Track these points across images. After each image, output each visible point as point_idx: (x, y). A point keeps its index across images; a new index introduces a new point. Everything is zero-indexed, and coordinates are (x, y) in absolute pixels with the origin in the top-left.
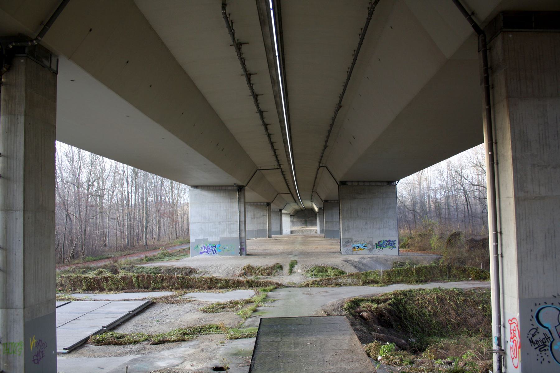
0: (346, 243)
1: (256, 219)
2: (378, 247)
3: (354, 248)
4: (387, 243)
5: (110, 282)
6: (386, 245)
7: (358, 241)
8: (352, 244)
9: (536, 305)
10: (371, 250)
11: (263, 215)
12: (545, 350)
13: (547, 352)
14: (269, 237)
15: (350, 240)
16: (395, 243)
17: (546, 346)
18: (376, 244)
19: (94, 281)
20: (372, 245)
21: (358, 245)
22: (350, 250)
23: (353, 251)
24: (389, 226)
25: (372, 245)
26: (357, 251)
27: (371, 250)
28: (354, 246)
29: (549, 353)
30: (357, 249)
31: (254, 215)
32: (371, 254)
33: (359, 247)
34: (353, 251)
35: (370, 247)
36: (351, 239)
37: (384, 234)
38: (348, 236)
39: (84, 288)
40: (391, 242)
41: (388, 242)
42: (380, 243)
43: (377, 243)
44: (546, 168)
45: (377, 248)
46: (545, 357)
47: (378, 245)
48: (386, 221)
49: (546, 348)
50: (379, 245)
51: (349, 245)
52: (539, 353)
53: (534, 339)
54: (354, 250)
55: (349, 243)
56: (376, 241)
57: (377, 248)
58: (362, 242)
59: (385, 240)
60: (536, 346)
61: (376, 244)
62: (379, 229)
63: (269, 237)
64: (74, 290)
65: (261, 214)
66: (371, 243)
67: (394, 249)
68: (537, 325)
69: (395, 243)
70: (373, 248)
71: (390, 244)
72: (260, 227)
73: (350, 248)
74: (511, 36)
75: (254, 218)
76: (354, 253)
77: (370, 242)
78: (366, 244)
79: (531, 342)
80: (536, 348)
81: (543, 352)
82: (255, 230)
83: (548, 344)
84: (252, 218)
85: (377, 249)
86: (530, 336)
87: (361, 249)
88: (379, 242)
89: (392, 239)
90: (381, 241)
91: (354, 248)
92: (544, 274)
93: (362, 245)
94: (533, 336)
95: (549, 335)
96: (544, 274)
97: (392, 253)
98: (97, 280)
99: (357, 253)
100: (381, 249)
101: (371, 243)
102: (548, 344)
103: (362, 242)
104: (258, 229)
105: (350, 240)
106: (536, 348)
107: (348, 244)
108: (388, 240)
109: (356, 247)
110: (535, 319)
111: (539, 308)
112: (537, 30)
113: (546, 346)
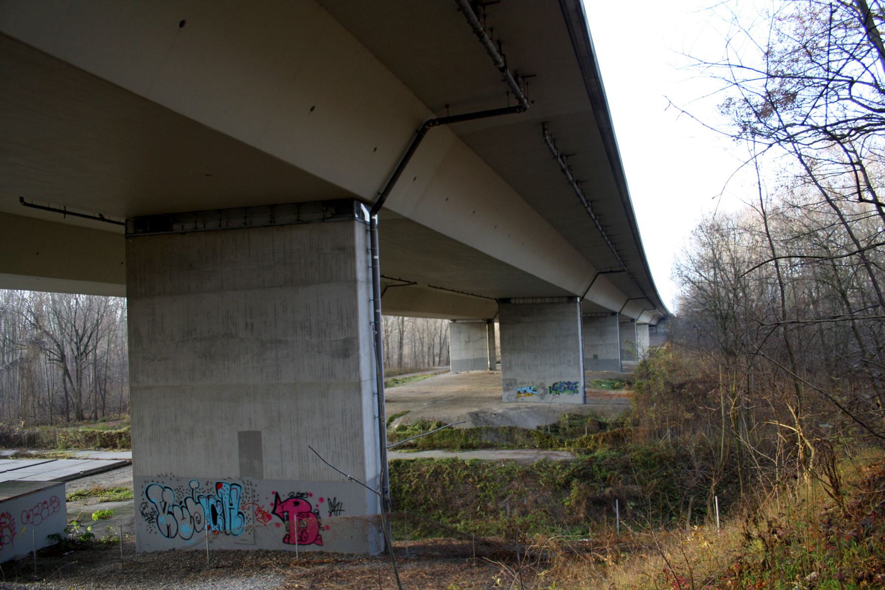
0: (507, 385)
1: (471, 343)
2: (553, 391)
3: (519, 392)
4: (565, 385)
5: (124, 439)
6: (565, 388)
7: (525, 383)
8: (515, 387)
9: (145, 482)
10: (542, 396)
11: (482, 338)
12: (153, 522)
13: (154, 524)
14: (491, 369)
15: (513, 382)
16: (577, 387)
17: (153, 518)
18: (550, 387)
19: (108, 437)
20: (544, 388)
21: (524, 389)
22: (513, 395)
23: (517, 397)
24: (569, 361)
25: (544, 388)
26: (523, 398)
27: (542, 396)
28: (519, 389)
29: (155, 524)
30: (523, 395)
31: (469, 337)
32: (543, 401)
33: (525, 391)
34: (517, 397)
35: (541, 391)
36: (513, 379)
37: (561, 373)
38: (509, 375)
39: (98, 444)
40: (571, 385)
41: (567, 384)
42: (556, 386)
43: (551, 385)
44: (153, 361)
45: (551, 392)
46: (153, 528)
47: (553, 389)
48: (564, 355)
49: (153, 520)
50: (555, 389)
51: (511, 389)
52: (148, 524)
53: (145, 512)
54: (519, 395)
55: (512, 385)
56: (549, 384)
57: (551, 392)
58: (531, 384)
59: (562, 381)
60: (146, 518)
61: (550, 387)
62: (554, 366)
63: (491, 369)
64: (87, 448)
65: (479, 335)
66: (542, 386)
67: (575, 394)
68: (146, 500)
69: (577, 387)
70: (545, 393)
71: (571, 387)
72: (477, 355)
73: (514, 392)
74: (131, 241)
75: (469, 342)
76: (520, 400)
77: (542, 384)
78: (535, 387)
79: (143, 514)
80: (146, 520)
81: (151, 524)
82: (471, 360)
83: (155, 517)
84: (466, 342)
85: (552, 394)
86: (142, 509)
87: (529, 395)
88: (554, 385)
89: (573, 380)
90: (557, 383)
91: (519, 392)
92: (151, 455)
93: (530, 388)
94: (144, 509)
95: (156, 510)
96: (151, 455)
97: (571, 401)
98: (110, 436)
99: (522, 400)
100: (557, 395)
101: (542, 386)
102: (155, 517)
103: (531, 384)
104: (476, 357)
105: (513, 382)
106: (146, 520)
107: (511, 387)
108: (566, 381)
109: (521, 392)
110: (145, 495)
111: (147, 486)
112: (151, 234)
113: (153, 518)
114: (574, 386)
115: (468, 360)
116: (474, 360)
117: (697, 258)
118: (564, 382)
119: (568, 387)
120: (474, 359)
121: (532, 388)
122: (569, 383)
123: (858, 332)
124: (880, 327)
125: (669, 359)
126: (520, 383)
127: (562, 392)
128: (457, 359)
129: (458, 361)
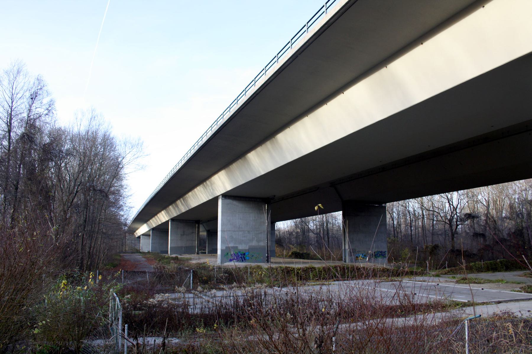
6: (380, 255)
7: (360, 252)
11: (193, 233)
31: (184, 232)
41: (381, 252)
82: (184, 247)
84: (181, 235)
89: (383, 250)
108: (380, 251)
114: (384, 253)
115: (181, 247)
116: (187, 247)
117: (108, 133)
118: (380, 251)
119: (381, 254)
120: (186, 247)
121: (364, 254)
122: (381, 252)
123: (3, 200)
124: (531, 207)
125: (503, 236)
126: (358, 252)
127: (378, 257)
128: (174, 246)
129: (175, 247)
